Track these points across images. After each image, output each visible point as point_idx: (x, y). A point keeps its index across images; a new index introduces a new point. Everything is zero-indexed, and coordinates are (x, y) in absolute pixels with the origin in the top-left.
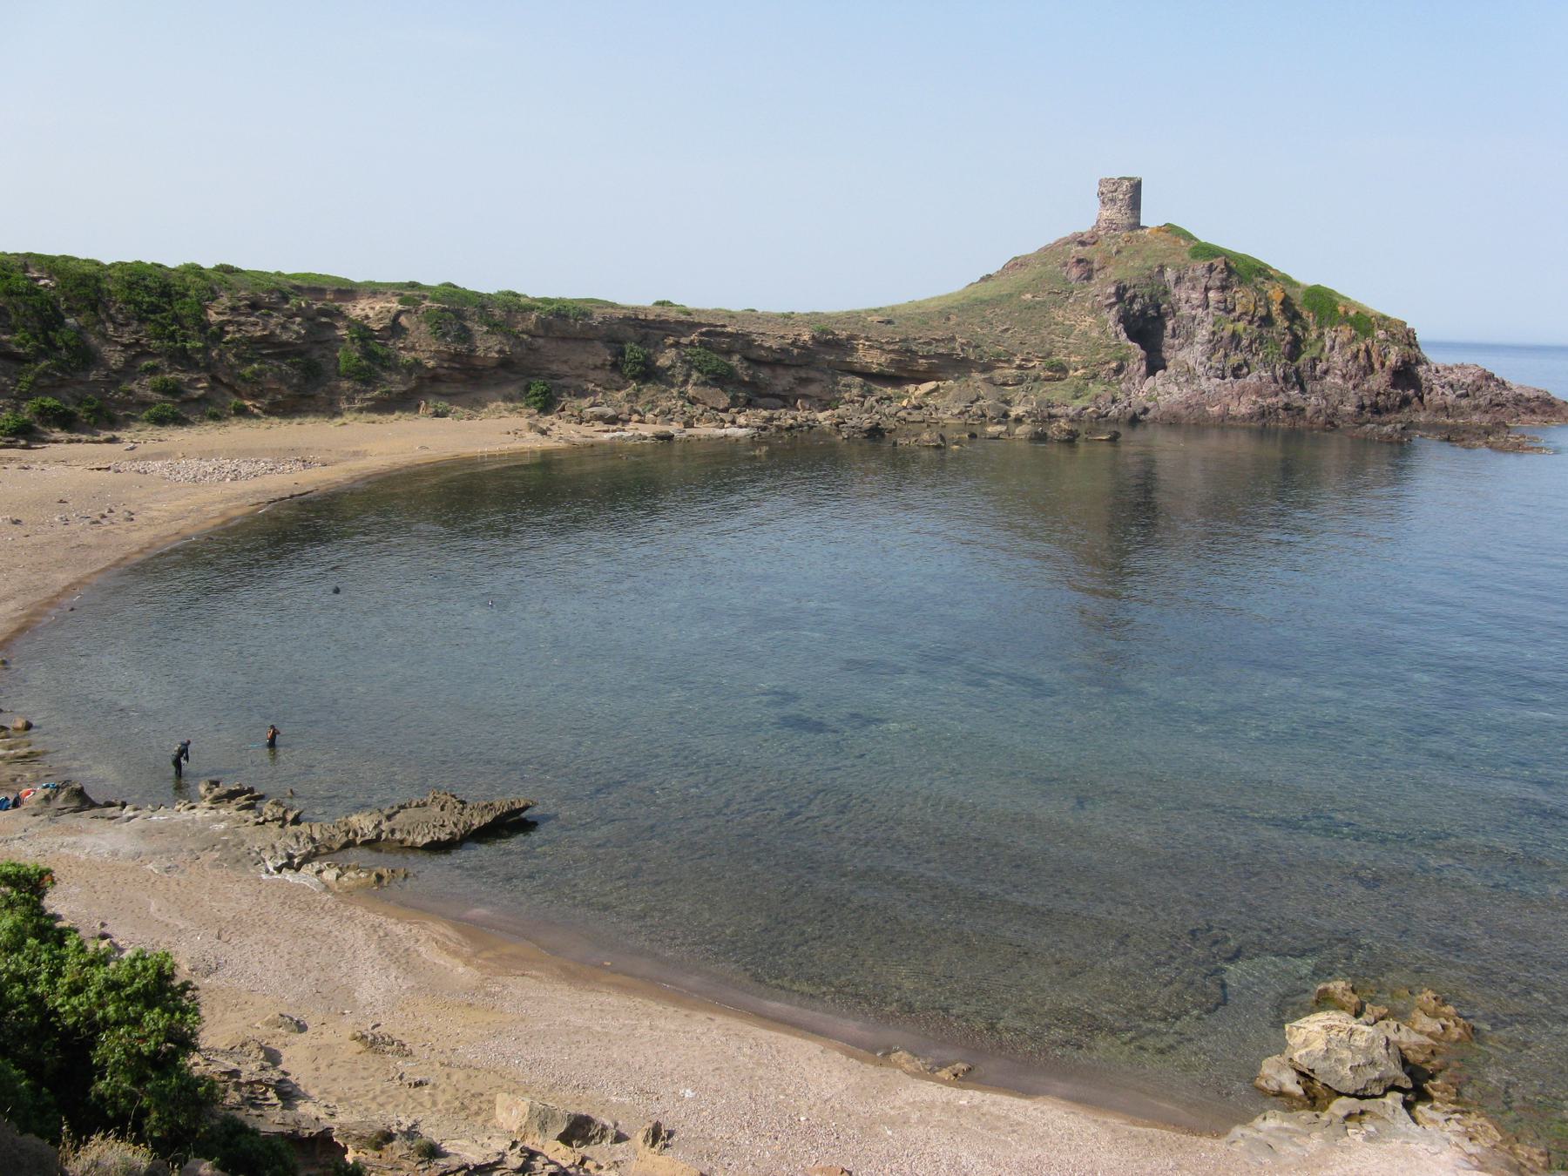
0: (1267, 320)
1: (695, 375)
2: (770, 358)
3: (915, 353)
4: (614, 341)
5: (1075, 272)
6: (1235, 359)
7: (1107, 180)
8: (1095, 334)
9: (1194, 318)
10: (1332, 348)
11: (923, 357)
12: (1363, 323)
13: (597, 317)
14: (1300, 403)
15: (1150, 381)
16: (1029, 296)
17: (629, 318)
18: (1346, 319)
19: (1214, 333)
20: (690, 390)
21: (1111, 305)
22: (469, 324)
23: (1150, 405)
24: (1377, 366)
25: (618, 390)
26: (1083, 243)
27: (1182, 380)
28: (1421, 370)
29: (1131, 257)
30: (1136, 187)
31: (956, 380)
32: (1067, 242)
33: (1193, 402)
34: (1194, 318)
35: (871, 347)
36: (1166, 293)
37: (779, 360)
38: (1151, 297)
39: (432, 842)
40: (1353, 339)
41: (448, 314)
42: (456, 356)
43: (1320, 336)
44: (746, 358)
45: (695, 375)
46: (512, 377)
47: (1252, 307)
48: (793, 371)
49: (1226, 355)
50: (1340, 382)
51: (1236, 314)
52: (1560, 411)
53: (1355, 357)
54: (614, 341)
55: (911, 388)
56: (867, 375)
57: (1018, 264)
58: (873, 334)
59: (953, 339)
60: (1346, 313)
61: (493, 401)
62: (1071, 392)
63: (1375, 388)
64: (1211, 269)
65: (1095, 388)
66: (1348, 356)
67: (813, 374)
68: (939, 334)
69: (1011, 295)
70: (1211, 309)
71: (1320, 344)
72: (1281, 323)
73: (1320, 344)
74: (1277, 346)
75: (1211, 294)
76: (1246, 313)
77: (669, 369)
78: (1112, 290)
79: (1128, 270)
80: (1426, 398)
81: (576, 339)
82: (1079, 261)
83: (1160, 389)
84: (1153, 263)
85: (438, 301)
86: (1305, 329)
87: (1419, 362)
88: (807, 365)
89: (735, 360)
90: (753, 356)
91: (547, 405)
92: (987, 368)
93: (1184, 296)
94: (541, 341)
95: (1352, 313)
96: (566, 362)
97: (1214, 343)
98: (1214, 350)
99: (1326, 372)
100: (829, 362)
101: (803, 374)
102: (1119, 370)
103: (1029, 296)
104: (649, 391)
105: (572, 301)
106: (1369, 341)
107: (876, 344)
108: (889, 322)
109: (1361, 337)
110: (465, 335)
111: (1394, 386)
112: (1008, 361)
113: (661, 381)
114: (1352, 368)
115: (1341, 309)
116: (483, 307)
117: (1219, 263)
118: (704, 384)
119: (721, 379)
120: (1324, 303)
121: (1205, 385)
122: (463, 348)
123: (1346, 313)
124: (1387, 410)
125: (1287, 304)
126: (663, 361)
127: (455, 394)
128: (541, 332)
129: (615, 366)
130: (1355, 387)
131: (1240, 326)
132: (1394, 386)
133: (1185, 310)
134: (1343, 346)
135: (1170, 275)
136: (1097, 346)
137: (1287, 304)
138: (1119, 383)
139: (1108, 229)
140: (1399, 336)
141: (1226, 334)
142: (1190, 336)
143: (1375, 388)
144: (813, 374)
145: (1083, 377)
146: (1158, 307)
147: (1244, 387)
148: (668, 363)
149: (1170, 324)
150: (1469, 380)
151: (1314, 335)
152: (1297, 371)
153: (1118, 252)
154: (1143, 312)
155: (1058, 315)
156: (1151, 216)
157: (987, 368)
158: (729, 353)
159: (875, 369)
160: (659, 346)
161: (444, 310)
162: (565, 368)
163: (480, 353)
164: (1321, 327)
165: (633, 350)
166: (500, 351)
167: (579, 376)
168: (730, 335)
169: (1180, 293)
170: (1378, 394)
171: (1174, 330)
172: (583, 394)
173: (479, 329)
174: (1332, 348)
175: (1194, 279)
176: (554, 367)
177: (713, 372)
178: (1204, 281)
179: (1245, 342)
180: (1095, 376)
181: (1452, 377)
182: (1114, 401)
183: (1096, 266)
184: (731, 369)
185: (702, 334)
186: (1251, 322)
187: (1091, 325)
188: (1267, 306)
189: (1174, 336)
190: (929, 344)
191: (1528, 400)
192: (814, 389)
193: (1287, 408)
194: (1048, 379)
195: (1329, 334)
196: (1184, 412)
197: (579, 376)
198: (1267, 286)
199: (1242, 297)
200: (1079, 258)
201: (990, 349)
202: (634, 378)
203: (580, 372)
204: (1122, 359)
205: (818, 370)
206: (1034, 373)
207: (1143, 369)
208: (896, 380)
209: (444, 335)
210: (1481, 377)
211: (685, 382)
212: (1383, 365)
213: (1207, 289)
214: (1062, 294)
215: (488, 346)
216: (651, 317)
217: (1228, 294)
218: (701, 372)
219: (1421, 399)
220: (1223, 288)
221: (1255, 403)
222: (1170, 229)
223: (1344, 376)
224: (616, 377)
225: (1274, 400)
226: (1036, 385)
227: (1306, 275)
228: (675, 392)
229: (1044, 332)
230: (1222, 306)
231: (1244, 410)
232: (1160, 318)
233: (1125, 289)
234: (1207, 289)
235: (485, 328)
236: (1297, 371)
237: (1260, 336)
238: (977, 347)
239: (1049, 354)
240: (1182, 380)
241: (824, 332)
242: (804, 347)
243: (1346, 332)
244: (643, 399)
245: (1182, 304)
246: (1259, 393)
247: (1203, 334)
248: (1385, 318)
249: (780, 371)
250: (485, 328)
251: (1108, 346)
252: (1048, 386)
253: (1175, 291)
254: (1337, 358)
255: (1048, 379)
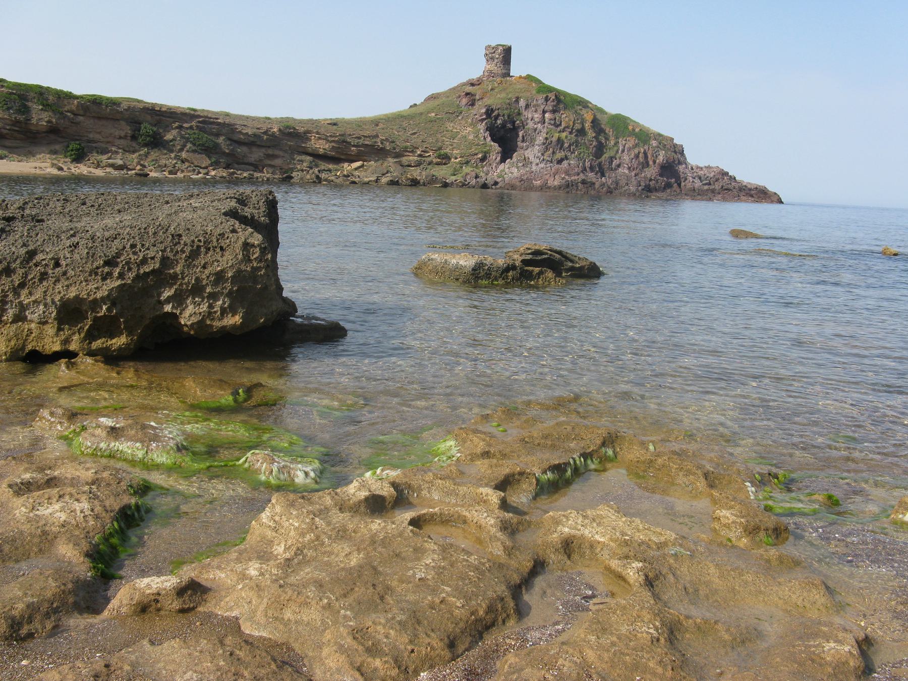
0: (582, 132)
1: (189, 145)
2: (246, 141)
3: (349, 143)
4: (136, 122)
5: (464, 101)
6: (559, 155)
7: (489, 46)
8: (471, 137)
9: (535, 130)
10: (623, 151)
11: (354, 146)
12: (644, 136)
13: (124, 106)
14: (594, 180)
15: (502, 166)
16: (433, 114)
17: (148, 109)
18: (633, 133)
19: (546, 139)
20: (184, 155)
21: (482, 120)
22: (30, 104)
23: (499, 180)
24: (651, 163)
25: (134, 152)
26: (473, 85)
27: (520, 165)
28: (681, 168)
29: (500, 92)
30: (507, 51)
31: (376, 161)
32: (464, 84)
33: (525, 177)
34: (535, 130)
35: (320, 138)
36: (519, 114)
37: (253, 142)
38: (509, 116)
39: (513, 598)
40: (636, 146)
41: (13, 97)
42: (16, 122)
43: (616, 144)
44: (230, 139)
45: (189, 145)
46: (60, 139)
47: (571, 123)
48: (263, 150)
49: (554, 153)
50: (627, 172)
51: (562, 127)
52: (769, 197)
53: (637, 156)
54: (136, 122)
55: (346, 165)
56: (316, 156)
57: (433, 97)
58: (322, 131)
59: (377, 136)
60: (633, 130)
61: (40, 153)
62: (451, 171)
63: (649, 176)
64: (547, 99)
65: (466, 169)
66: (632, 156)
67: (277, 152)
68: (367, 133)
69: (421, 114)
70: (546, 124)
71: (616, 148)
72: (591, 134)
73: (616, 148)
74: (588, 148)
75: (547, 115)
76: (568, 127)
77: (171, 141)
78: (484, 110)
79: (495, 100)
80: (683, 184)
81: (107, 119)
82: (467, 94)
83: (507, 170)
84: (513, 96)
85: (10, 88)
86: (607, 139)
87: (680, 163)
88: (275, 147)
89: (221, 140)
90: (235, 138)
91: (79, 158)
92: (398, 155)
93: (530, 116)
94: (81, 118)
95: (637, 130)
96: (100, 133)
97: (547, 145)
98: (547, 149)
99: (619, 166)
100: (290, 146)
101: (270, 152)
102: (483, 159)
103: (433, 114)
104: (154, 154)
105: (241, 117)
106: (646, 147)
107: (323, 137)
108: (335, 124)
109: (641, 144)
110: (25, 110)
111: (661, 175)
112: (412, 152)
113: (165, 148)
114: (635, 163)
115: (630, 128)
116: (41, 94)
117: (552, 96)
118: (194, 151)
119: (209, 150)
120: (621, 123)
121: (534, 168)
122: (21, 118)
123: (633, 130)
124: (656, 190)
125: (595, 122)
126: (169, 137)
127: (17, 148)
128: (81, 112)
129: (134, 138)
130: (636, 175)
131: (564, 135)
132: (661, 175)
133: (531, 125)
134: (630, 149)
135: (522, 103)
136: (471, 144)
137: (595, 122)
138: (483, 167)
139: (489, 76)
140: (668, 146)
141: (554, 139)
142: (533, 140)
143: (649, 176)
144: (277, 152)
145: (460, 163)
146: (514, 122)
147: (558, 169)
148: (171, 137)
149: (521, 134)
150: (712, 175)
151: (612, 143)
152: (600, 164)
153: (492, 89)
154: (504, 125)
155: (450, 126)
156: (517, 69)
157: (398, 155)
158: (217, 135)
159: (321, 151)
160: (167, 128)
161: (11, 94)
162: (98, 137)
163: (34, 121)
164: (617, 138)
165: (146, 128)
166: (49, 122)
167: (108, 142)
168: (219, 124)
169: (528, 114)
170: (651, 180)
171: (523, 137)
172: (104, 152)
173: (35, 107)
174: (623, 151)
175: (536, 106)
176: (91, 136)
177: (203, 145)
178: (542, 107)
179: (566, 145)
180: (467, 163)
181: (701, 173)
182: (477, 177)
183: (477, 97)
184: (217, 146)
185: (199, 122)
186: (571, 133)
187: (471, 132)
188: (582, 123)
189: (523, 141)
190: (359, 138)
191: (750, 190)
192: (278, 162)
193: (584, 182)
194: (438, 164)
195: (621, 141)
196: (518, 184)
197: (108, 142)
198: (584, 111)
199: (566, 117)
200: (469, 93)
201: (401, 144)
202: (146, 145)
203: (110, 139)
204: (486, 153)
205: (281, 150)
206: (429, 159)
207: (499, 158)
208: (336, 160)
209: (8, 109)
210: (719, 173)
211: (181, 150)
212: (654, 162)
213: (544, 112)
214: (455, 114)
215: (40, 117)
216: (163, 109)
217: (557, 115)
218: (194, 145)
219: (679, 185)
220: (554, 111)
221: (563, 179)
222: (530, 78)
223: (629, 168)
224: (134, 144)
225: (576, 177)
226: (430, 167)
227: (612, 109)
228: (173, 155)
229: (439, 136)
230: (552, 122)
231: (556, 183)
232: (515, 130)
233: (492, 111)
234: (544, 112)
235: (41, 107)
236: (600, 164)
237: (577, 141)
238: (393, 142)
239: (440, 149)
240: (520, 165)
241: (288, 127)
242: (273, 134)
243: (631, 142)
244: (150, 158)
245: (529, 121)
246: (567, 173)
247: (540, 139)
248: (660, 135)
249: (254, 149)
250: (41, 107)
251: (478, 145)
252: (437, 168)
253: (525, 113)
254: (626, 158)
255: (438, 164)
